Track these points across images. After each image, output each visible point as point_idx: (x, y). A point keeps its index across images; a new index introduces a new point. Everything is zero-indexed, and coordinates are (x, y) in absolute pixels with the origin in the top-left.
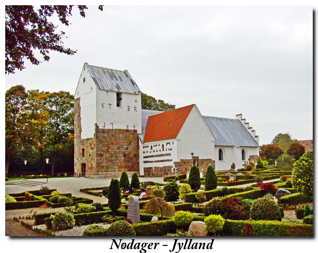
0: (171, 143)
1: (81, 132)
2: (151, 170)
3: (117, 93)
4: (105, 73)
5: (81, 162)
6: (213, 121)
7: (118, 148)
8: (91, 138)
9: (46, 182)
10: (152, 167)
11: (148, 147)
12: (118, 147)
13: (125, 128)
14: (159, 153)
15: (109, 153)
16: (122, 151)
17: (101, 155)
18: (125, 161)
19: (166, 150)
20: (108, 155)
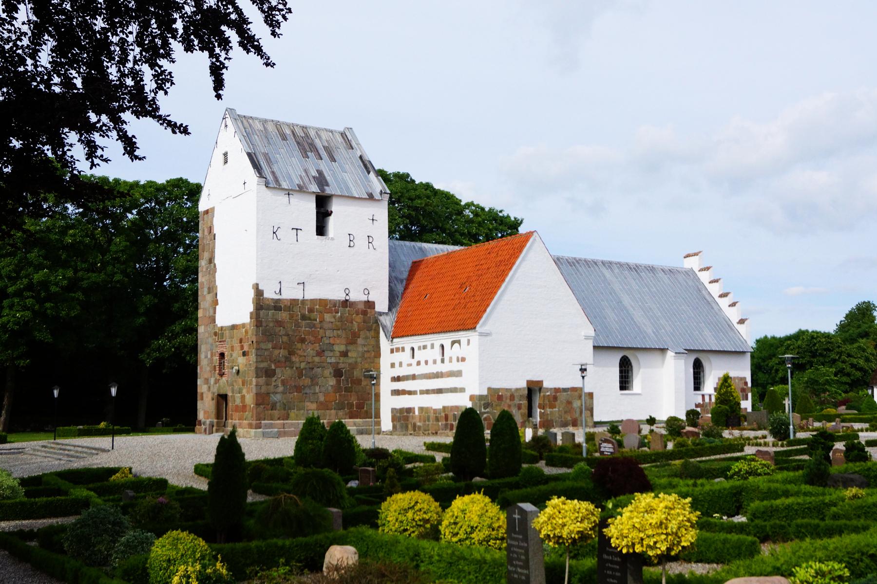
0: (464, 341)
1: (217, 307)
2: (411, 414)
3: (316, 197)
4: (284, 137)
5: (215, 390)
6: (607, 273)
7: (320, 353)
8: (243, 325)
9: (109, 447)
10: (414, 408)
11: (403, 349)
12: (318, 348)
13: (341, 296)
14: (432, 369)
15: (293, 368)
16: (329, 360)
17: (269, 374)
18: (337, 389)
19: (451, 360)
20: (288, 372)
